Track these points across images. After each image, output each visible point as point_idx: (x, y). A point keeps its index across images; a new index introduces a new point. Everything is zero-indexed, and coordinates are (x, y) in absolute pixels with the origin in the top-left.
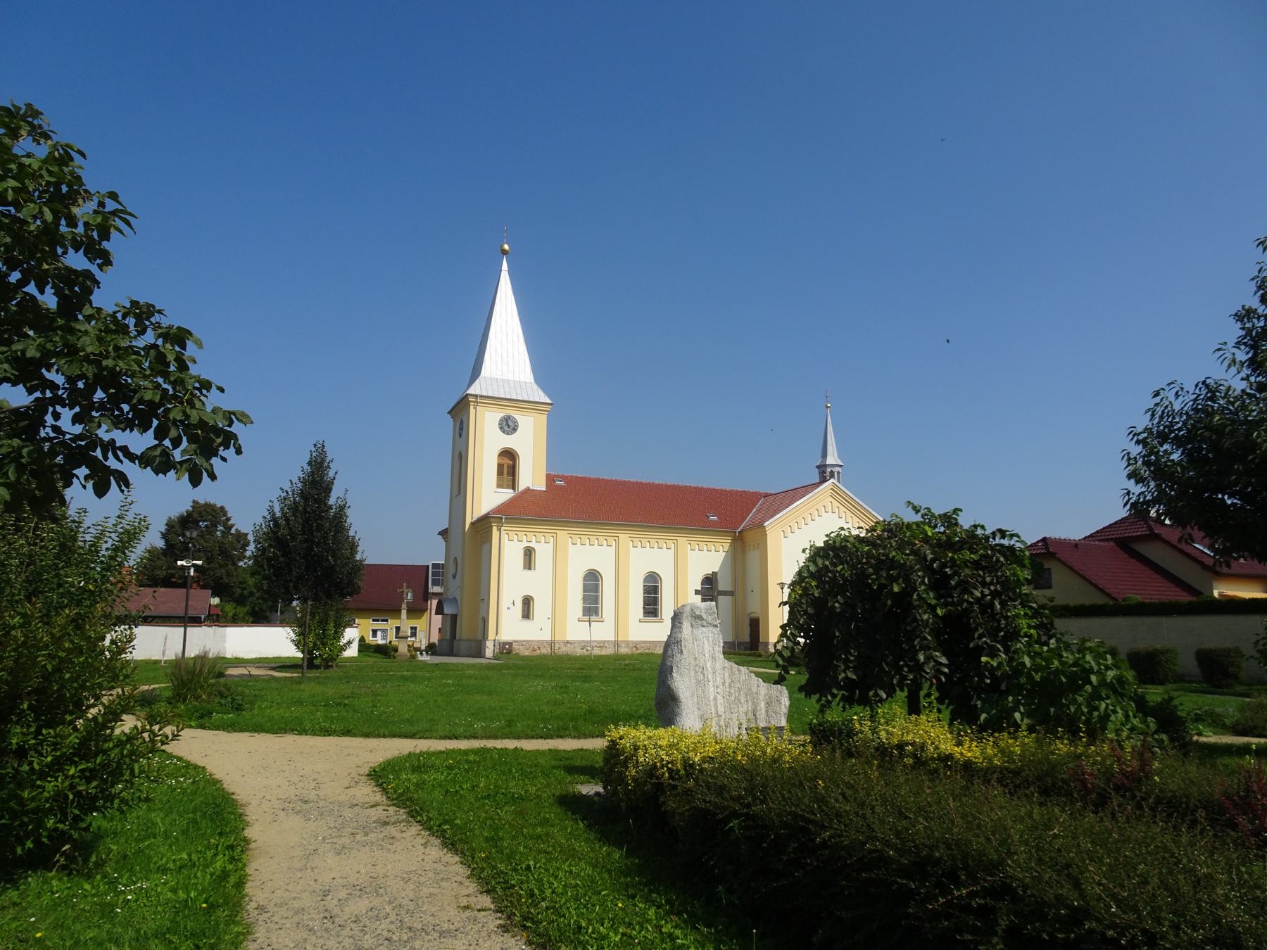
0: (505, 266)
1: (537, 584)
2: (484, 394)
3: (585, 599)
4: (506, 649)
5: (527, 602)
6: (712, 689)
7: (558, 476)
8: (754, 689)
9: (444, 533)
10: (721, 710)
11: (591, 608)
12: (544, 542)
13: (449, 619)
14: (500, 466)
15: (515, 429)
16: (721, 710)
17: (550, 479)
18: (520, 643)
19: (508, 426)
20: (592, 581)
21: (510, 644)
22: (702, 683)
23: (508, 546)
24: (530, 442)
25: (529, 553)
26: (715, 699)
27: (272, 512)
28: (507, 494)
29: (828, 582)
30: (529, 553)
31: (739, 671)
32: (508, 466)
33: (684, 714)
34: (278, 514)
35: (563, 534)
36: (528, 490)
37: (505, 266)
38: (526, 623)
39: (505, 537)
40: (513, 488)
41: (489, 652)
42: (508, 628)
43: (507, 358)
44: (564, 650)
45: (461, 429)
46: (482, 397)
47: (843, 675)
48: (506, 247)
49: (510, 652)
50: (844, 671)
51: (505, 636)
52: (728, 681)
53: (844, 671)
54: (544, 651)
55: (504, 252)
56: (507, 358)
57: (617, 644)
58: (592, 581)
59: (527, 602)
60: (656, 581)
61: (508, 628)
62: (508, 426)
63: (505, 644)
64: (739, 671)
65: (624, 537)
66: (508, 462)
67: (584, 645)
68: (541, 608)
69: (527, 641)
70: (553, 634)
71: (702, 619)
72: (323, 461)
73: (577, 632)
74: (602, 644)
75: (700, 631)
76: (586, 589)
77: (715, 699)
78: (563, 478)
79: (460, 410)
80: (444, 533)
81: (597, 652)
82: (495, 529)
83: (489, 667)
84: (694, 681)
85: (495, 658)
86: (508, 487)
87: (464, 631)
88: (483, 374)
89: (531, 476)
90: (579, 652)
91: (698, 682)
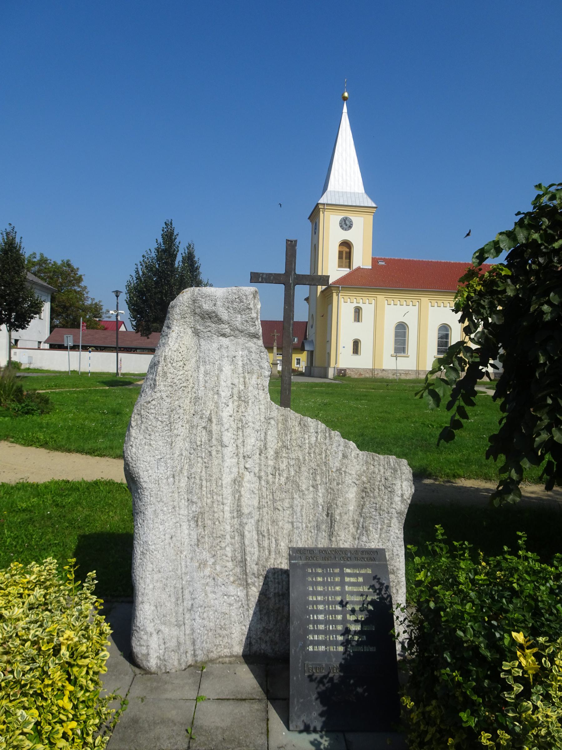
0: (345, 109)
1: (363, 331)
2: (329, 202)
3: (396, 342)
4: (342, 374)
5: (356, 344)
6: (230, 461)
7: (381, 259)
8: (335, 463)
9: (307, 299)
10: (249, 502)
11: (401, 347)
12: (369, 303)
13: (309, 352)
14: (340, 253)
15: (350, 227)
16: (249, 502)
17: (375, 261)
18: (351, 369)
19: (346, 224)
20: (401, 330)
21: (345, 370)
22: (207, 444)
23: (344, 306)
24: (361, 235)
25: (358, 311)
26: (237, 482)
27: (137, 272)
28: (345, 271)
29: (536, 273)
30: (358, 311)
31: (304, 427)
32: (346, 253)
33: (149, 512)
34: (141, 273)
35: (381, 298)
36: (359, 268)
37: (345, 109)
38: (356, 357)
39: (341, 300)
40: (350, 267)
41: (331, 373)
42: (343, 359)
43: (346, 175)
44: (381, 375)
45: (315, 229)
46: (328, 205)
47: (544, 436)
48: (346, 94)
49: (344, 375)
50: (548, 428)
51: (342, 365)
52: (273, 444)
53: (548, 428)
54: (367, 376)
55: (345, 99)
56: (346, 175)
57: (373, 370)
58: (401, 330)
59: (356, 344)
60: (447, 330)
61: (343, 359)
62: (346, 224)
63: (341, 370)
64: (304, 427)
65: (425, 300)
66: (346, 249)
67: (395, 372)
68: (366, 347)
69: (357, 369)
70: (418, 365)
71: (220, 321)
72: (172, 233)
73: (390, 364)
74: (407, 372)
75: (213, 346)
76: (397, 335)
77: (237, 482)
78: (384, 260)
79: (314, 216)
80: (307, 299)
81: (403, 377)
82: (334, 294)
83: (329, 385)
84: (181, 444)
85: (334, 379)
86: (345, 267)
87: (316, 363)
88: (329, 189)
89: (362, 259)
90: (391, 377)
91: (195, 447)
